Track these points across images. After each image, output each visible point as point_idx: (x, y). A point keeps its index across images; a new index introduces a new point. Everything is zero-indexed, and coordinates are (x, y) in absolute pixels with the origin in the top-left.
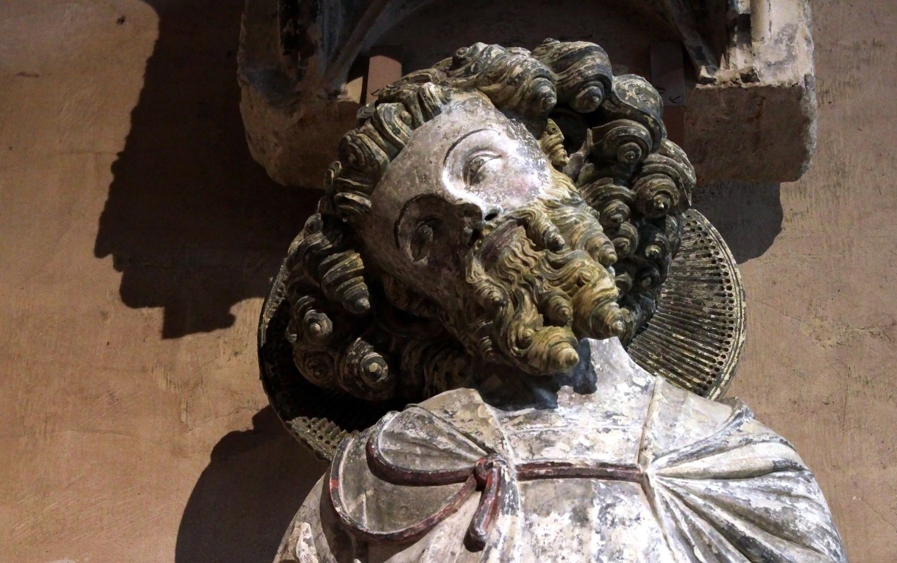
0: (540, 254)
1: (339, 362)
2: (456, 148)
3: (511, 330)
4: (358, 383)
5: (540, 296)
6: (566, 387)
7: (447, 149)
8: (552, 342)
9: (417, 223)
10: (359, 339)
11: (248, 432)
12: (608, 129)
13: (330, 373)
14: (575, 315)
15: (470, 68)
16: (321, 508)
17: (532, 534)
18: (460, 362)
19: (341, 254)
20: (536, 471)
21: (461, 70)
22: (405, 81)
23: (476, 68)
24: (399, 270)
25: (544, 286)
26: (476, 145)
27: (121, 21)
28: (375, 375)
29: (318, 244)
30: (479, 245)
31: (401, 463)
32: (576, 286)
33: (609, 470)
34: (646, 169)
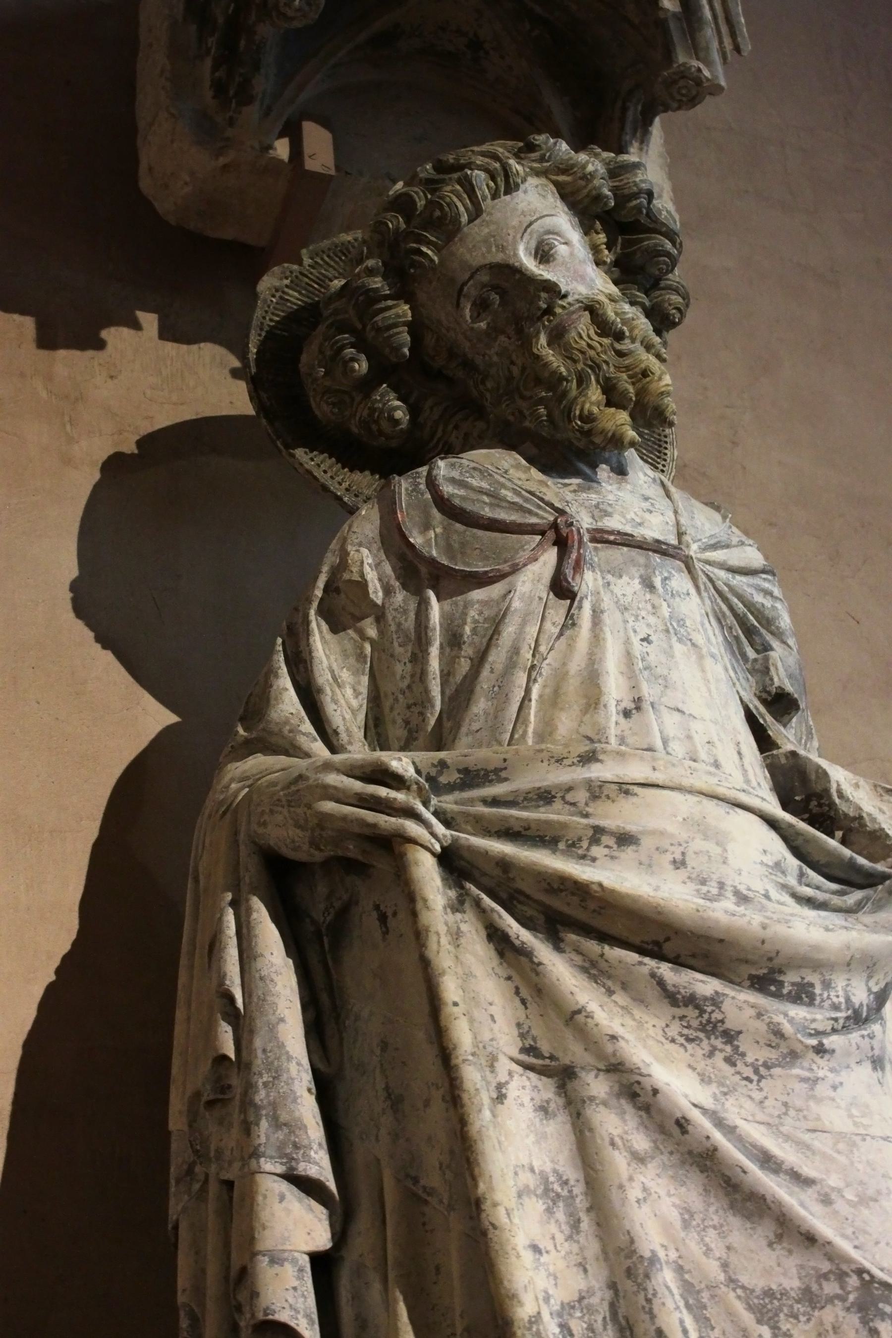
0: (606, 341)
1: (360, 403)
2: (532, 227)
3: (577, 404)
4: (374, 427)
5: (607, 379)
6: (604, 466)
7: (525, 225)
8: (619, 423)
9: (482, 289)
10: (385, 385)
11: (132, 455)
12: (642, 240)
13: (347, 413)
14: (637, 403)
15: (545, 155)
16: (381, 535)
17: (612, 592)
18: (481, 425)
19: (395, 302)
20: (606, 536)
21: (535, 155)
22: (470, 153)
23: (550, 157)
24: (448, 330)
26: (549, 228)
28: (397, 422)
29: (377, 288)
30: (549, 321)
31: (469, 507)
32: (640, 376)
33: (664, 547)
34: (663, 284)
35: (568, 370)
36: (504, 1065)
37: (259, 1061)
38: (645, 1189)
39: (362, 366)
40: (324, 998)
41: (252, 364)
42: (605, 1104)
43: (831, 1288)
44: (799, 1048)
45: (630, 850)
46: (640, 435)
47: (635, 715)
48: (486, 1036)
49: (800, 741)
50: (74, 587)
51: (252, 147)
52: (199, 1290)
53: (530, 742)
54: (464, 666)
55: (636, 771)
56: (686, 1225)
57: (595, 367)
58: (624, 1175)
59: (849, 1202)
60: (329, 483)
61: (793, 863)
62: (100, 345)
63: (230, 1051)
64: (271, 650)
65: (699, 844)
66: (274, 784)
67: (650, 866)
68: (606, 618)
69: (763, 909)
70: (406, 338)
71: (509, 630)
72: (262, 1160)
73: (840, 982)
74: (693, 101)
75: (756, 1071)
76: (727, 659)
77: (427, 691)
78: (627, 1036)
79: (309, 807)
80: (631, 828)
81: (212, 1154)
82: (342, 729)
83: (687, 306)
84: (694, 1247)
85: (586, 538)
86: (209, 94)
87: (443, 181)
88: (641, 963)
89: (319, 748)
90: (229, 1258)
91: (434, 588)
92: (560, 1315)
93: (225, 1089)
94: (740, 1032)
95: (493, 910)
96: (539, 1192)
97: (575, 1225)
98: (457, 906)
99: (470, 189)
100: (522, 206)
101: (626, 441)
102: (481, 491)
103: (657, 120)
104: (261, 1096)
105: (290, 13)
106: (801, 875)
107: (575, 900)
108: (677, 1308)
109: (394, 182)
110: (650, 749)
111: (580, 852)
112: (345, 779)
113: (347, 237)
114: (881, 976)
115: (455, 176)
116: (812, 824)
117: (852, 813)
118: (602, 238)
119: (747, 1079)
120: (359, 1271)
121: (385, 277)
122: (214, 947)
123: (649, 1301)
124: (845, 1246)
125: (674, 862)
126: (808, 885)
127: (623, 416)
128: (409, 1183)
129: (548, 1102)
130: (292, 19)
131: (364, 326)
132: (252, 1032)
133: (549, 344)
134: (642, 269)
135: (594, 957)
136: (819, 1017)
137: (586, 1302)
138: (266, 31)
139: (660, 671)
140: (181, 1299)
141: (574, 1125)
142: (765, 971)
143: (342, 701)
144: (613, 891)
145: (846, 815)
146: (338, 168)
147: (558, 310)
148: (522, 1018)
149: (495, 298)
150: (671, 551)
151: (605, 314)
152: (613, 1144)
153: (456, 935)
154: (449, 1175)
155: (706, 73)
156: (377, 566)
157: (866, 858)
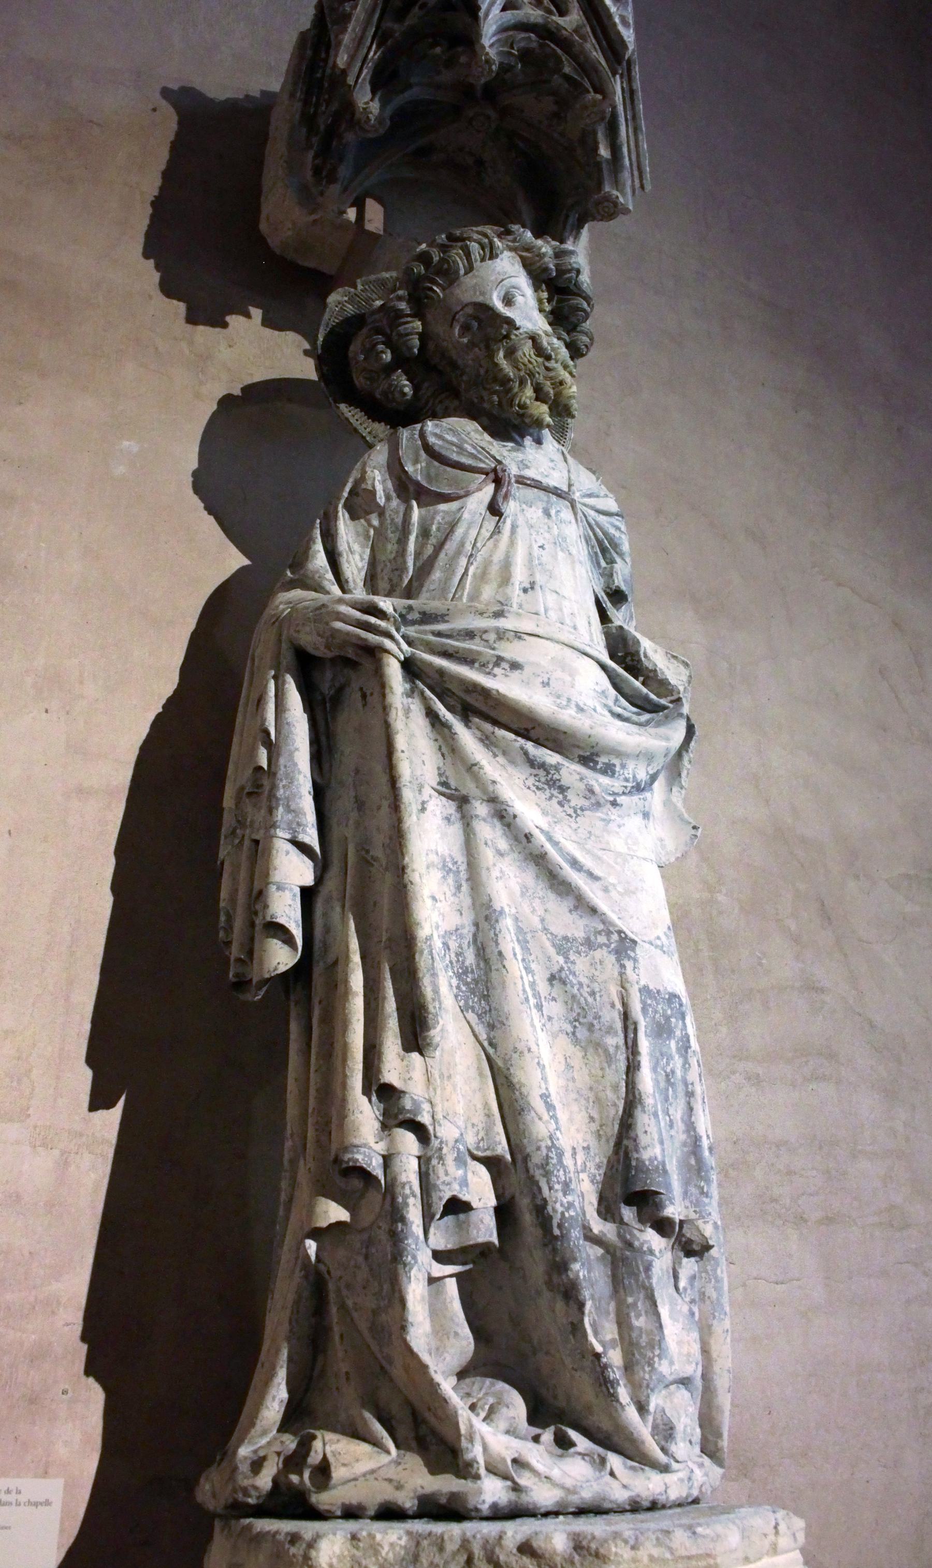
0: (540, 360)
4: (390, 396)
5: (538, 384)
6: (528, 437)
11: (238, 396)
12: (569, 300)
18: (456, 403)
25: (541, 379)
27: (154, 110)
28: (405, 394)
31: (444, 452)
34: (579, 329)
35: (514, 374)
36: (427, 791)
37: (281, 772)
38: (501, 871)
39: (387, 357)
40: (323, 739)
41: (319, 347)
42: (484, 820)
43: (602, 939)
44: (602, 801)
45: (517, 673)
46: (553, 421)
47: (530, 591)
48: (419, 773)
49: (625, 621)
50: (195, 474)
51: (333, 211)
52: (233, 900)
53: (465, 600)
54: (429, 550)
55: (526, 625)
56: (523, 894)
57: (531, 374)
58: (491, 863)
59: (618, 892)
60: (359, 427)
61: (612, 692)
62: (225, 325)
63: (264, 764)
64: (312, 527)
65: (559, 674)
66: (306, 608)
67: (528, 683)
68: (519, 530)
69: (591, 717)
70: (416, 342)
71: (459, 531)
72: (278, 830)
73: (631, 765)
74: (610, 216)
75: (575, 812)
76: (588, 565)
77: (405, 562)
78: (502, 782)
79: (327, 624)
80: (520, 659)
81: (248, 824)
82: (350, 580)
83: (592, 344)
84: (526, 909)
85: (513, 480)
86: (309, 174)
87: (451, 246)
88: (515, 740)
89: (336, 590)
90: (252, 883)
91: (416, 499)
92: (444, 937)
93: (260, 786)
94: (569, 788)
95: (431, 699)
96: (440, 866)
97: (459, 888)
98: (410, 694)
99: (468, 254)
100: (498, 269)
101: (545, 423)
102: (452, 444)
103: (586, 226)
104: (280, 793)
105: (367, 127)
106: (616, 700)
107: (480, 698)
108: (512, 941)
109: (420, 244)
110: (536, 614)
111: (487, 670)
112: (350, 609)
113: (386, 275)
114: (655, 765)
115: (459, 244)
116: (626, 669)
117: (651, 667)
118: (545, 295)
119: (570, 815)
120: (328, 900)
121: (408, 302)
122: (260, 702)
123: (496, 935)
124: (613, 917)
125: (543, 683)
126: (619, 706)
127: (544, 408)
128: (363, 853)
129: (451, 815)
130: (368, 131)
131: (392, 332)
132: (279, 755)
133: (505, 357)
134: (567, 318)
135: (488, 733)
136: (616, 784)
137: (459, 932)
138: (350, 137)
139: (549, 567)
140: (222, 904)
141: (465, 831)
142: (588, 754)
143: (353, 562)
144: (504, 696)
145: (647, 668)
146: (385, 230)
147: (513, 337)
148: (441, 765)
149: (475, 324)
150: (563, 495)
151: (541, 342)
152: (486, 844)
153: (407, 711)
154: (388, 851)
155: (621, 200)
156: (383, 482)
157: (655, 694)
